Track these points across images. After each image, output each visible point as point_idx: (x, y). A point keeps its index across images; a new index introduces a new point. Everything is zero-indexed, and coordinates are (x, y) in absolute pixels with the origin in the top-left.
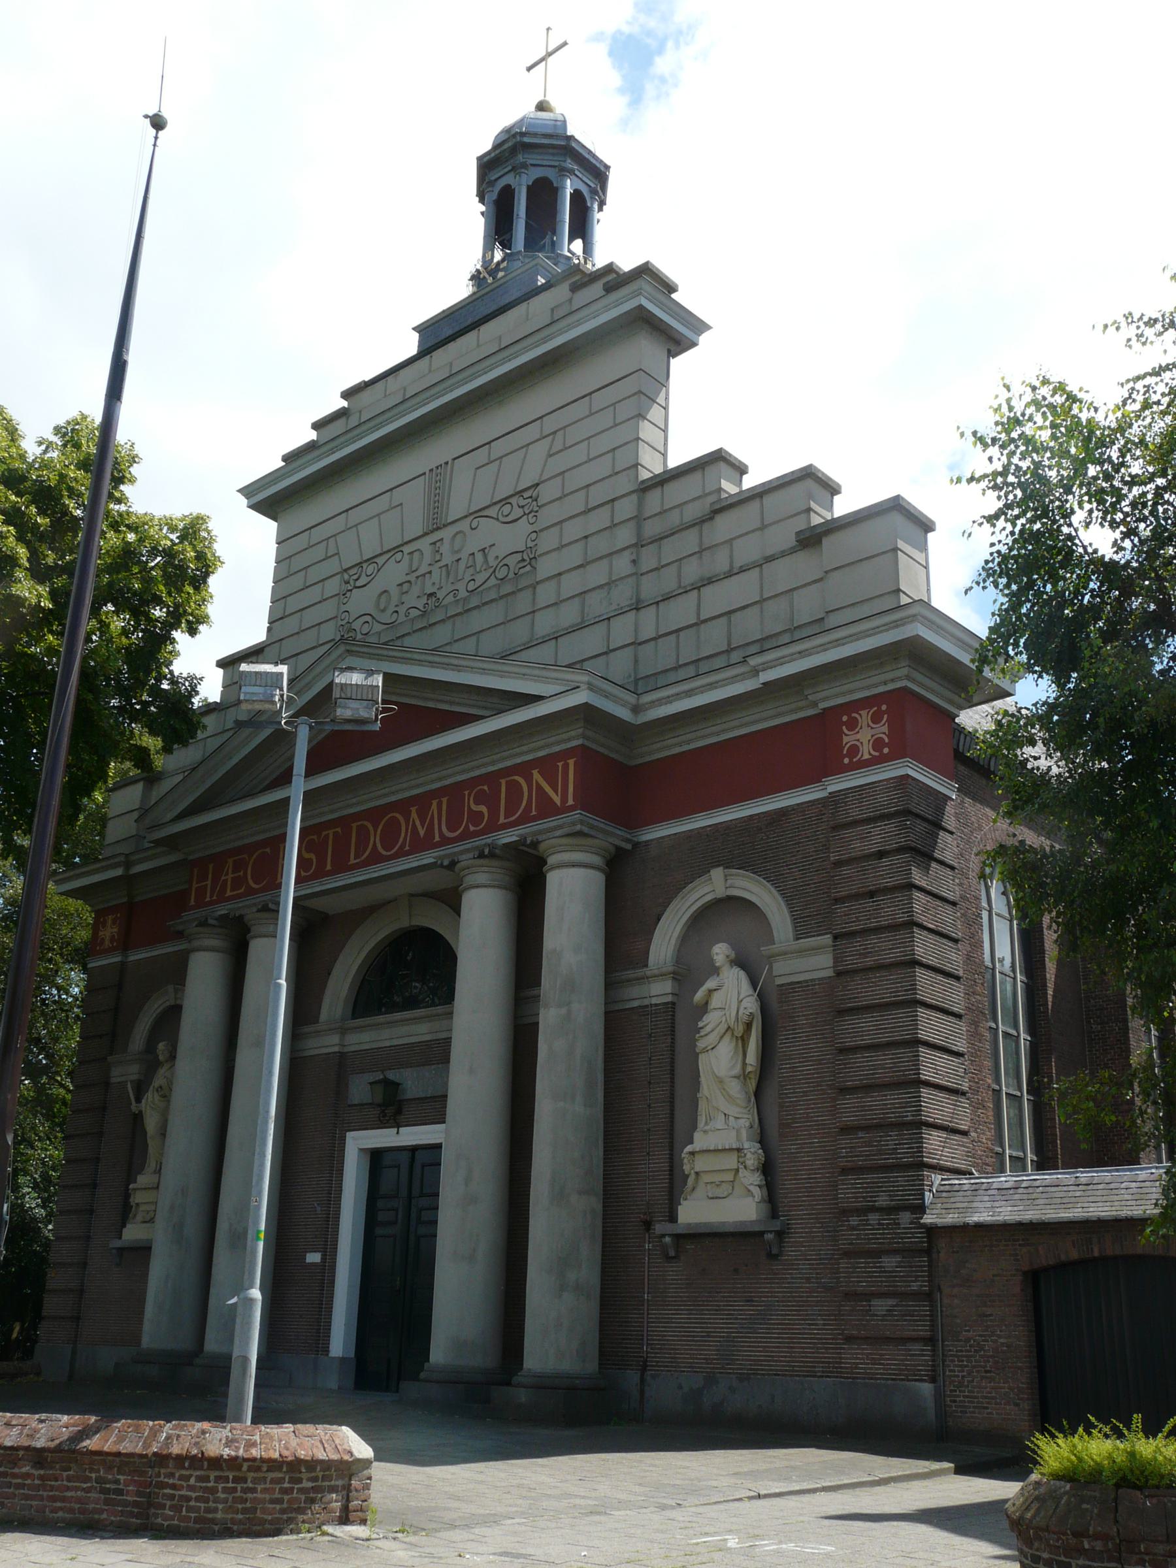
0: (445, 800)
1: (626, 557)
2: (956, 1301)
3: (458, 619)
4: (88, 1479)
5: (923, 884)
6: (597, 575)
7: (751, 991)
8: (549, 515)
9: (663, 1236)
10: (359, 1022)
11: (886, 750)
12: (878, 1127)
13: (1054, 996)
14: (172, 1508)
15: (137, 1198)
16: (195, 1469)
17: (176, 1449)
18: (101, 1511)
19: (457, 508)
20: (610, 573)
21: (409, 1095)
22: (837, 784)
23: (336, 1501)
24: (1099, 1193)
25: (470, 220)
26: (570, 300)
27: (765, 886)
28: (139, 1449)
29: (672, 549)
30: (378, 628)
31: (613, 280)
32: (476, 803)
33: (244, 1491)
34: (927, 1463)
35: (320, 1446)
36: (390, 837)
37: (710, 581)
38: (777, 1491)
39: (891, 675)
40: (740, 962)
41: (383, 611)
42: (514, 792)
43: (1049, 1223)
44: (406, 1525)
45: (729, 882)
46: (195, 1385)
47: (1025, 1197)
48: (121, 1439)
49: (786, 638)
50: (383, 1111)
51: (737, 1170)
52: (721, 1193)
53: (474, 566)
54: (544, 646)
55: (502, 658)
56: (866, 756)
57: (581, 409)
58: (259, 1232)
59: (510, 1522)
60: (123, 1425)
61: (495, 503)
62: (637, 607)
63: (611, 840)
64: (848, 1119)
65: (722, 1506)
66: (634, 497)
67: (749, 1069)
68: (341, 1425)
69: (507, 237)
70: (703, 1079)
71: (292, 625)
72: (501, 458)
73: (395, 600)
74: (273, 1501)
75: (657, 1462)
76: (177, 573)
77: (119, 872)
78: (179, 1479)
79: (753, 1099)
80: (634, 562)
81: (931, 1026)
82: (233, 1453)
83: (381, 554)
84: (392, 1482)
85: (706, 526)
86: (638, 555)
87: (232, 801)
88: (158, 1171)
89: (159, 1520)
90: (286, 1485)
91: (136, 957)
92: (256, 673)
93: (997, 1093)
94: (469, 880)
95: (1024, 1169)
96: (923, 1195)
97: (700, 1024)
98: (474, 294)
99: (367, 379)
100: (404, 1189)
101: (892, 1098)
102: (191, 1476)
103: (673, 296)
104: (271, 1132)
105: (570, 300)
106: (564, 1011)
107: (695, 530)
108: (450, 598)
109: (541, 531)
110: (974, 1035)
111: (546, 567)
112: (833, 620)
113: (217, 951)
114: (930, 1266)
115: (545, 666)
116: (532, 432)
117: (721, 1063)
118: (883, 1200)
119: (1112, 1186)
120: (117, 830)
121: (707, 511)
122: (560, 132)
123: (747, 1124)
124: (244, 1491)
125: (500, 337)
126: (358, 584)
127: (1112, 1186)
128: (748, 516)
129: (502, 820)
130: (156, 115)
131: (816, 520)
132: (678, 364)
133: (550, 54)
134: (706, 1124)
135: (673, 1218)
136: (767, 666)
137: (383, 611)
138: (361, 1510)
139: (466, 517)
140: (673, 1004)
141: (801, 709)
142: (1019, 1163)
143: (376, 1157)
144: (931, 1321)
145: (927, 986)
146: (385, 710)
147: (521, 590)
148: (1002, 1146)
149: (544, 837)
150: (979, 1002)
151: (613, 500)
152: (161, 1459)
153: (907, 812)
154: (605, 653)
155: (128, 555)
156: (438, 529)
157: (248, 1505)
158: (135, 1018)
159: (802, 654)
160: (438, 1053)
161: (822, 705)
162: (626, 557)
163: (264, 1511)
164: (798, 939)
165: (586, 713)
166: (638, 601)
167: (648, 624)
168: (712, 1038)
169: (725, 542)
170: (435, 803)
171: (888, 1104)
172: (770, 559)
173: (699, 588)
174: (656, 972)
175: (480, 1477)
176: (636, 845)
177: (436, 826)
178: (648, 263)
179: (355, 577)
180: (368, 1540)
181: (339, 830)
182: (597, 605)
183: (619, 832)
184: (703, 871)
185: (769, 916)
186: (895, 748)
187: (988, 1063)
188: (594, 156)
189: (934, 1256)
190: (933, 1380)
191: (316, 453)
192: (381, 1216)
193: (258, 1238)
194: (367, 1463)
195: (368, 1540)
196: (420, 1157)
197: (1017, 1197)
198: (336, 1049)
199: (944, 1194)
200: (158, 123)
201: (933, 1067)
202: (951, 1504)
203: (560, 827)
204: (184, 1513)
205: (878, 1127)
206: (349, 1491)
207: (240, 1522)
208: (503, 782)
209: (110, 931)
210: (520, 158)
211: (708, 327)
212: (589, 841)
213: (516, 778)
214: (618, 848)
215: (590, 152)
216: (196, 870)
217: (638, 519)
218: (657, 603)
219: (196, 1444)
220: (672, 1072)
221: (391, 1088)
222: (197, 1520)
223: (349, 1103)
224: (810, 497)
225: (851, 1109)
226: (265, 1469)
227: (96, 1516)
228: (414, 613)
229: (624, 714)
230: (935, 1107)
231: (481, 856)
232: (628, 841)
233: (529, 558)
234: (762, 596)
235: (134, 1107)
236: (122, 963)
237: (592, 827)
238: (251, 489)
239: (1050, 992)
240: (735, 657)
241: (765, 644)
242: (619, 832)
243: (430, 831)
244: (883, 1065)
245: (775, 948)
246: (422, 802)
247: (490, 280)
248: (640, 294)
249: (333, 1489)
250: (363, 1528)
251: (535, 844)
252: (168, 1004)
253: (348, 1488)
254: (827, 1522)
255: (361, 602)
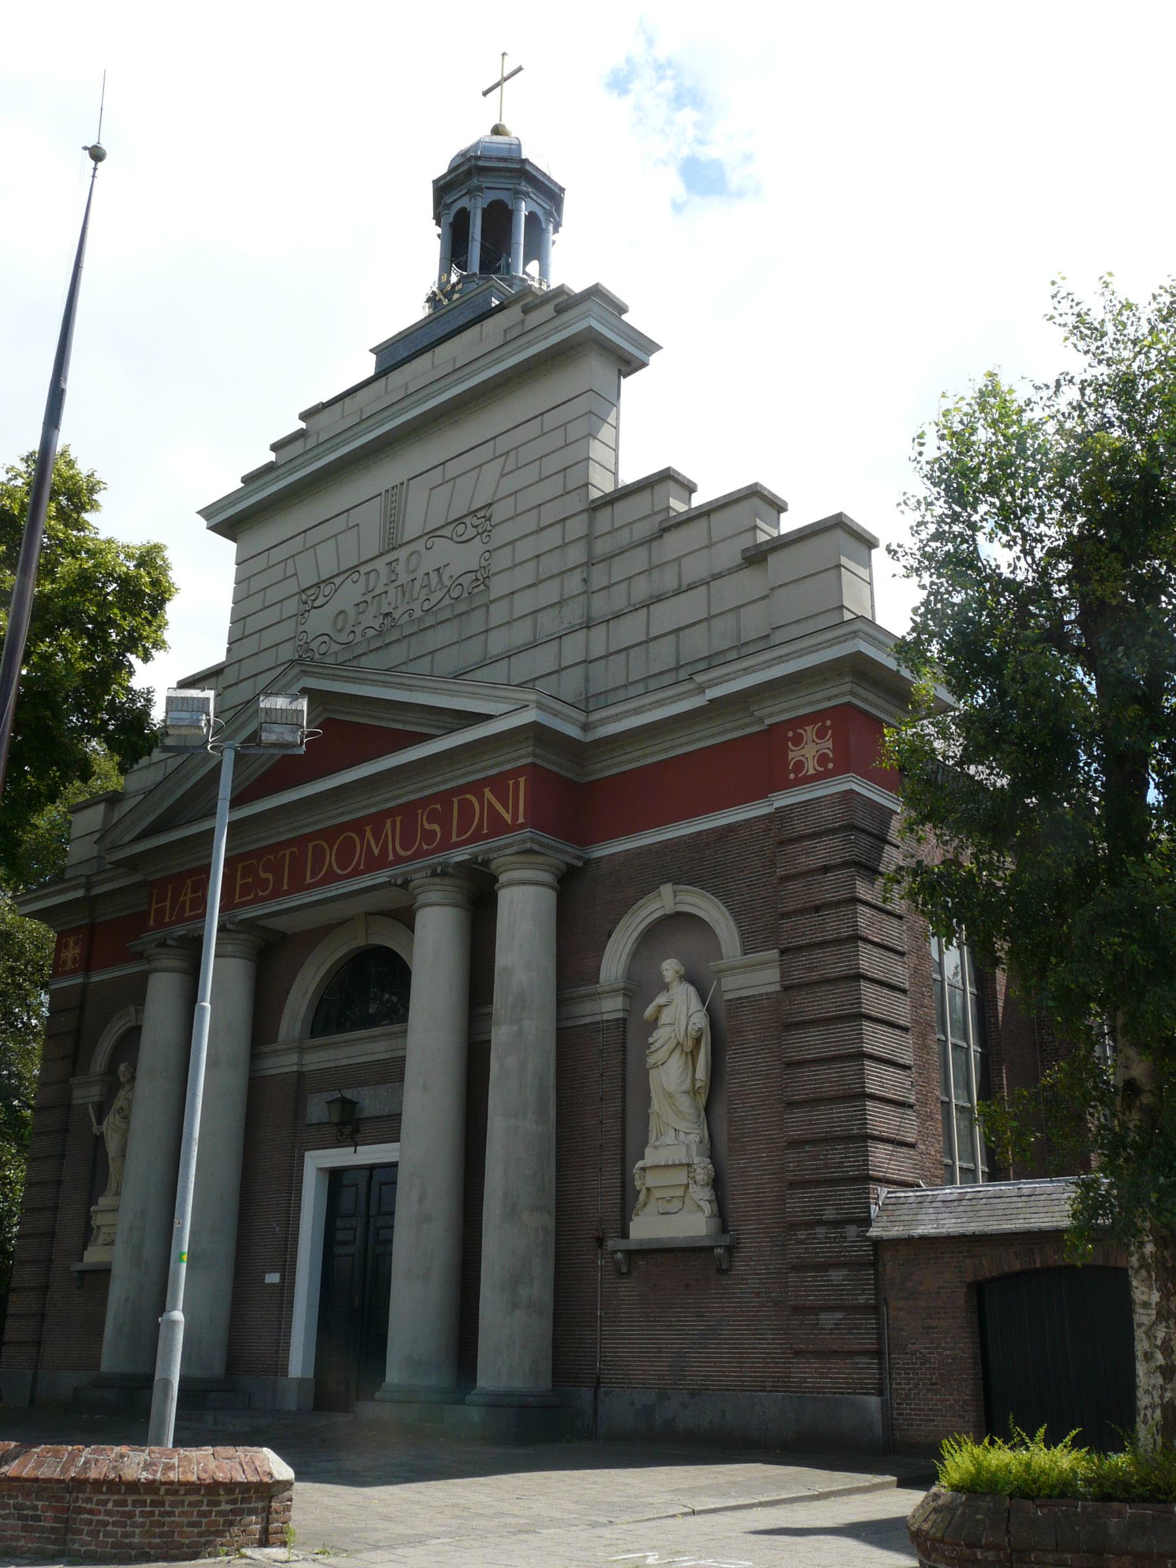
0: (398, 819)
1: (578, 576)
2: (902, 1314)
3: (414, 639)
4: (7, 1506)
5: (868, 898)
6: (549, 593)
7: (700, 1007)
8: (501, 535)
9: (616, 1252)
10: (318, 1041)
11: (830, 766)
12: (825, 1140)
13: (1004, 1008)
14: (89, 1533)
15: (98, 1220)
16: (112, 1493)
17: (93, 1474)
18: (18, 1538)
19: (412, 529)
20: (562, 591)
21: (365, 1114)
22: (783, 800)
23: (256, 1523)
24: (1041, 1204)
25: (428, 241)
26: (523, 321)
27: (713, 902)
28: (56, 1474)
29: (622, 568)
30: (335, 648)
31: (563, 301)
32: (429, 822)
33: (161, 1514)
34: (869, 1477)
35: (239, 1468)
36: (345, 857)
37: (659, 599)
38: (712, 1507)
39: (835, 691)
40: (690, 977)
41: (340, 631)
42: (466, 810)
43: (991, 1235)
44: (326, 1547)
45: (678, 898)
46: (122, 1410)
47: (969, 1208)
48: (39, 1465)
49: (733, 655)
50: (340, 1130)
51: (687, 1186)
52: (672, 1211)
53: (429, 585)
54: (498, 664)
55: (454, 678)
56: (812, 772)
57: (533, 428)
58: (181, 1254)
59: (434, 1542)
60: (42, 1450)
61: (449, 524)
62: (588, 625)
63: (562, 857)
64: (795, 1133)
65: (653, 1523)
66: (585, 516)
67: (699, 1084)
68: (262, 1446)
69: (462, 259)
70: (653, 1094)
71: (250, 646)
72: (455, 478)
73: (351, 621)
74: (190, 1525)
75: (600, 1480)
76: (138, 597)
77: (80, 893)
78: (97, 1504)
79: (703, 1114)
80: (585, 580)
81: (876, 1040)
82: (151, 1477)
83: (338, 575)
84: (316, 1504)
85: (655, 544)
86: (588, 575)
87: (190, 822)
88: (118, 1194)
89: (76, 1546)
90: (205, 1508)
91: (97, 979)
92: (183, 698)
93: (946, 1105)
94: (422, 898)
95: (975, 1180)
96: (869, 1208)
97: (651, 1040)
98: (430, 315)
99: (324, 401)
100: (361, 1206)
101: (838, 1112)
102: (109, 1500)
103: (624, 317)
104: (195, 1154)
105: (523, 321)
106: (515, 1028)
107: (645, 548)
108: (406, 618)
109: (495, 550)
110: (922, 1047)
111: (498, 587)
112: (778, 637)
113: (173, 971)
114: (876, 1279)
115: (494, 685)
116: (485, 452)
117: (671, 1080)
118: (830, 1214)
119: (1054, 1197)
120: (77, 852)
121: (656, 528)
122: (514, 155)
123: (697, 1139)
124: (161, 1514)
125: (454, 359)
126: (316, 604)
127: (1054, 1197)
128: (695, 534)
129: (454, 839)
130: (95, 147)
131: (762, 538)
132: (628, 384)
133: (505, 79)
134: (657, 1139)
135: (625, 1234)
136: (713, 683)
137: (340, 631)
138: (282, 1532)
139: (421, 537)
140: (624, 1020)
141: (747, 725)
142: (969, 1175)
143: (335, 1177)
144: (878, 1334)
145: (872, 999)
146: (310, 734)
147: (473, 609)
148: (952, 1158)
149: (495, 855)
150: (926, 1014)
151: (564, 520)
152: (79, 1484)
153: (852, 827)
154: (557, 671)
155: (85, 581)
156: (394, 549)
157: (166, 1529)
158: (96, 1040)
159: (747, 671)
160: (392, 1072)
161: (768, 722)
162: (578, 576)
163: (181, 1534)
164: (746, 954)
165: (536, 731)
166: (589, 619)
167: (599, 641)
168: (662, 1055)
169: (674, 560)
170: (389, 822)
171: (833, 1117)
172: (717, 577)
173: (648, 606)
174: (607, 988)
175: (417, 1497)
176: (587, 862)
177: (390, 846)
178: (597, 285)
179: (313, 597)
180: (286, 1562)
181: (295, 849)
182: (549, 623)
183: (569, 849)
184: (651, 887)
185: (718, 931)
186: (840, 763)
187: (936, 1076)
188: (549, 178)
189: (881, 1269)
190: (880, 1393)
191: (273, 475)
192: (340, 1236)
193: (180, 1260)
194: (287, 1485)
195: (286, 1562)
196: (378, 1176)
197: (960, 1209)
198: (295, 1068)
199: (890, 1207)
200: (97, 154)
201: (878, 1080)
202: (884, 1517)
203: (511, 845)
204: (101, 1538)
205: (825, 1140)
206: (269, 1513)
207: (157, 1546)
208: (455, 800)
209: (72, 952)
210: (475, 181)
211: (659, 348)
212: (541, 859)
213: (469, 796)
214: (569, 865)
215: (544, 175)
216: (155, 891)
217: (589, 538)
218: (608, 621)
219: (115, 1468)
220: (624, 1088)
221: (348, 1107)
222: (114, 1546)
223: (308, 1122)
224: (757, 515)
225: (798, 1123)
226: (182, 1492)
227: (14, 1544)
228: (371, 633)
229: (573, 732)
230: (880, 1119)
231: (434, 874)
232: (579, 858)
233: (483, 578)
234: (709, 612)
235: (95, 1129)
236: (85, 987)
237: (542, 845)
238: (209, 511)
239: (1001, 1004)
240: (683, 674)
241: (712, 660)
242: (569, 849)
243: (384, 850)
244: (828, 1078)
245: (724, 963)
246: (377, 821)
247: (446, 302)
248: (590, 315)
249: (252, 1511)
250: (283, 1550)
251: (486, 863)
252: (128, 1025)
253: (268, 1510)
254: (754, 1537)
255: (319, 622)
